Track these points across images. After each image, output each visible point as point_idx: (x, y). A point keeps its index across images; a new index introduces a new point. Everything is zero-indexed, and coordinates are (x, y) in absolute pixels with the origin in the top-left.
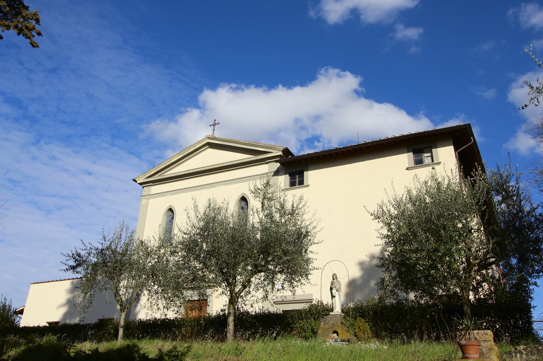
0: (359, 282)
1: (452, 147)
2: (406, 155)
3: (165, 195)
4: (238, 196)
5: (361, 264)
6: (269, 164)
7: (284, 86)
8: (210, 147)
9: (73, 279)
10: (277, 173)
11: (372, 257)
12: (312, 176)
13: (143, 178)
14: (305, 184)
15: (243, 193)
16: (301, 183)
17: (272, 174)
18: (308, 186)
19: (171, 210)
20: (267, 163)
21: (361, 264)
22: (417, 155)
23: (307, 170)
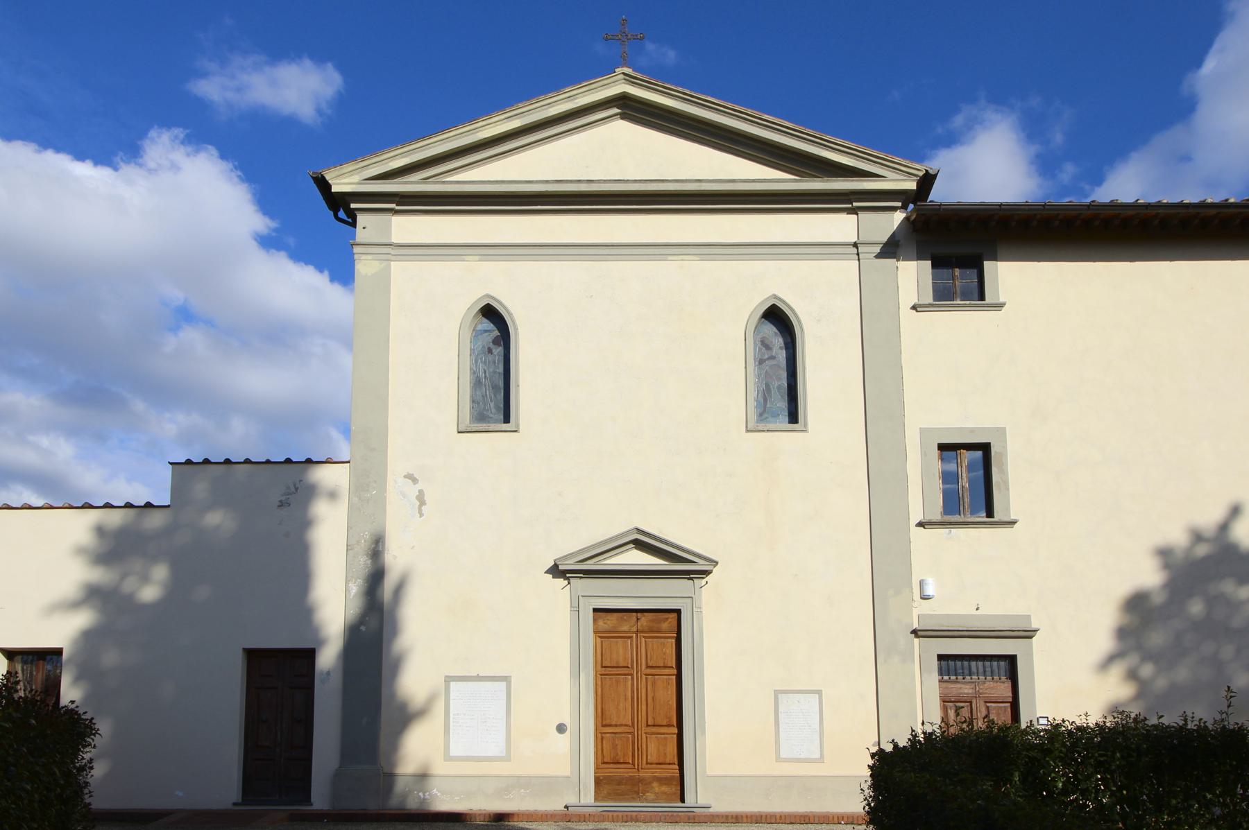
0: (1158, 599)
1: (929, 262)
2: (914, 263)
3: (663, 257)
4: (757, 302)
5: (1165, 554)
6: (861, 215)
7: (312, 58)
8: (624, 117)
9: (108, 506)
10: (891, 249)
11: (1197, 537)
12: (1008, 276)
13: (356, 178)
14: (988, 300)
15: (488, 296)
16: (978, 293)
17: (877, 249)
18: (1000, 306)
19: (490, 313)
20: (854, 211)
21: (1165, 554)
22: (946, 272)
23: (995, 258)
